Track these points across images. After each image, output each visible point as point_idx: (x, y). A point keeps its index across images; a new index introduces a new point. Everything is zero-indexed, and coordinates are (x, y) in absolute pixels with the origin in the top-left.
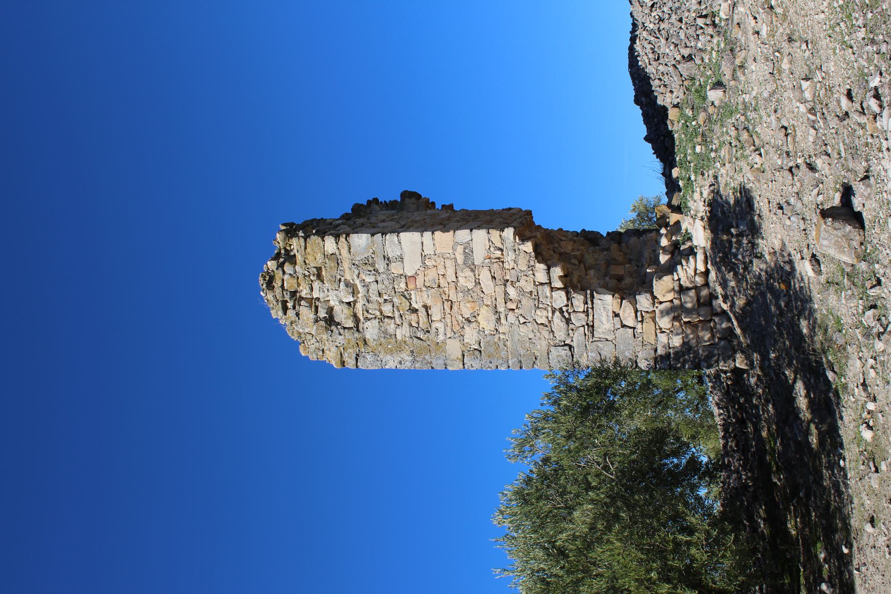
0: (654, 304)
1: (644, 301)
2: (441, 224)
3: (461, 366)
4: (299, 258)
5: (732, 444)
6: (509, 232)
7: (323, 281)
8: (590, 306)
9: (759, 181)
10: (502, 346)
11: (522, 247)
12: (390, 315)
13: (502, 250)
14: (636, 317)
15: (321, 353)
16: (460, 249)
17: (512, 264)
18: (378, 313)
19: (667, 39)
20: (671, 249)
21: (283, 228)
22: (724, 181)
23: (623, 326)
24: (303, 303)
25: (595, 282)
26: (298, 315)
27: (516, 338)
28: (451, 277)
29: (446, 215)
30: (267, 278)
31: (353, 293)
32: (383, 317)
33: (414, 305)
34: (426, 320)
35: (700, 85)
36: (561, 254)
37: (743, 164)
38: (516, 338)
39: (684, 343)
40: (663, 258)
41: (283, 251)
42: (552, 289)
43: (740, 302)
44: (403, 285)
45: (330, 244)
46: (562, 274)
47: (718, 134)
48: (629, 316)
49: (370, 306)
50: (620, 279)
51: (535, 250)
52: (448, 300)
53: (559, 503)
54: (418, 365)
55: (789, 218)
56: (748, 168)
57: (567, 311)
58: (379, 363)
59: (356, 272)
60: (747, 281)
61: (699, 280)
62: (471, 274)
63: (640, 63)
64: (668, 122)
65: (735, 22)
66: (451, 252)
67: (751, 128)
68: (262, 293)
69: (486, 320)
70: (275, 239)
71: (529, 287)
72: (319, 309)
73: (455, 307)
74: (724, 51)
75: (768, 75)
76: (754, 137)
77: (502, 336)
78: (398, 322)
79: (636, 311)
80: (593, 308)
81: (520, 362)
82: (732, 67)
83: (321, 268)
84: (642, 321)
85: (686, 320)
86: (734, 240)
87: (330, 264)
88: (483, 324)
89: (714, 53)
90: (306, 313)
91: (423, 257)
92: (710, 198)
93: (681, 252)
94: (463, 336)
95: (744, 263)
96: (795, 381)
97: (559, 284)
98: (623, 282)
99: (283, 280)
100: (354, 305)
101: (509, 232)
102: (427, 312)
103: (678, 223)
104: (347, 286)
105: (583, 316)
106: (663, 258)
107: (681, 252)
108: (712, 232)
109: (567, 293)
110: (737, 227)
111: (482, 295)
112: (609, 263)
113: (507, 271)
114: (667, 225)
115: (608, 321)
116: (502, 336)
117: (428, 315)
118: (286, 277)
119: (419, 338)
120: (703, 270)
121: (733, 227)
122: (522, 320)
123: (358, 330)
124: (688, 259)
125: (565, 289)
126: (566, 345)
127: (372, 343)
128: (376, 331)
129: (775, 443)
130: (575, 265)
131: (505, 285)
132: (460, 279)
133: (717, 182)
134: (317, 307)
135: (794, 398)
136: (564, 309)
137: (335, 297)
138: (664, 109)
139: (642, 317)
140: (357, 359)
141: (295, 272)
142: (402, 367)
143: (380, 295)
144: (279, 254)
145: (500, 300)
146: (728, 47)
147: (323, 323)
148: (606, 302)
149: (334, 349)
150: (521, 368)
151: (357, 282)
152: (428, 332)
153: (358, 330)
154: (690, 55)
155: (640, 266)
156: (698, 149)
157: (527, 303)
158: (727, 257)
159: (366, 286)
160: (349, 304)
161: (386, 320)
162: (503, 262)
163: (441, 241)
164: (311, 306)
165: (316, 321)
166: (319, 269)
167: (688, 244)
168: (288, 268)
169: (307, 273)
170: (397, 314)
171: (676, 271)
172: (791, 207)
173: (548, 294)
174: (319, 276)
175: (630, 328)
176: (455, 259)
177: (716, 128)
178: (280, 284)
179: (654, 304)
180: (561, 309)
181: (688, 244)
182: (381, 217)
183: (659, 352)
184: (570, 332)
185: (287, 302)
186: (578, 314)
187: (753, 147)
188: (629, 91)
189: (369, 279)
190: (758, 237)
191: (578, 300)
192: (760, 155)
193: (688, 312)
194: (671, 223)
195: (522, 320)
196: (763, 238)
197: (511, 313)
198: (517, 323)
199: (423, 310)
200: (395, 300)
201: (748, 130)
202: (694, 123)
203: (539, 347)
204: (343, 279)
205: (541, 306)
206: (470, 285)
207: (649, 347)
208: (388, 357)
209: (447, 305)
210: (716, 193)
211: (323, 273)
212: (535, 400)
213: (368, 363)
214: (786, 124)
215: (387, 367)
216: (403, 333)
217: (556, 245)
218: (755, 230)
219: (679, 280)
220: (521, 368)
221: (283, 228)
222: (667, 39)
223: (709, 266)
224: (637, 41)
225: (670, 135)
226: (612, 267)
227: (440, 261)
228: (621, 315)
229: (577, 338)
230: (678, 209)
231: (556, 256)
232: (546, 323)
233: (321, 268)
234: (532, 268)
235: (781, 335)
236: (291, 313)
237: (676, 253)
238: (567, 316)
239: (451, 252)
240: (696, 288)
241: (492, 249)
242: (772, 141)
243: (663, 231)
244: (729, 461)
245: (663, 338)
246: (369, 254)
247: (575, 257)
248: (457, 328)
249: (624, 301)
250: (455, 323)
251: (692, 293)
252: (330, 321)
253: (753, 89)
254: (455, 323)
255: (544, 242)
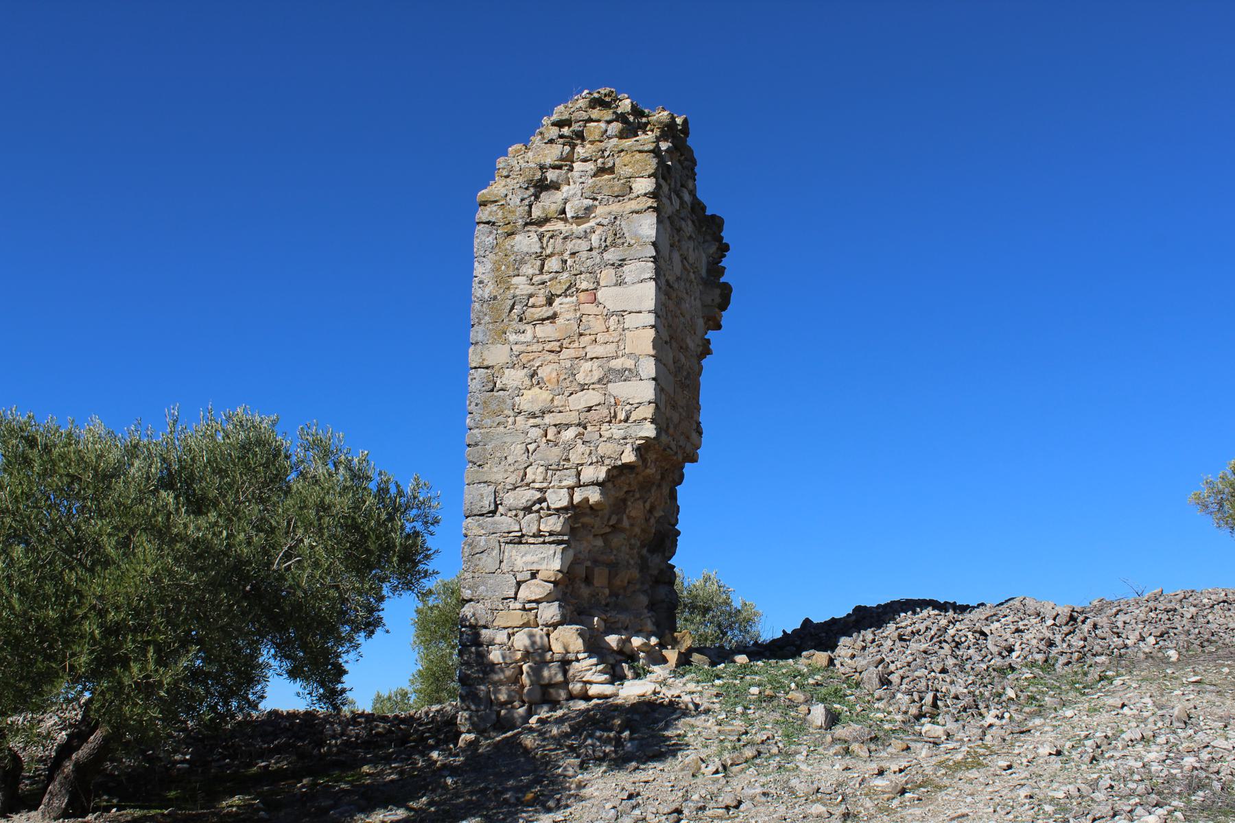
0: (546, 625)
1: (550, 612)
2: (671, 338)
3: (473, 365)
4: (627, 143)
5: (381, 727)
6: (649, 431)
7: (595, 175)
8: (547, 539)
9: (682, 770)
10: (498, 419)
11: (629, 448)
12: (546, 268)
13: (626, 421)
14: (530, 602)
15: (505, 173)
16: (629, 363)
17: (606, 434)
18: (548, 251)
19: (925, 652)
20: (626, 650)
21: (679, 121)
22: (698, 723)
23: (519, 584)
24: (567, 148)
25: (584, 546)
26: (551, 141)
27: (508, 439)
28: (592, 351)
29: (691, 345)
30: (607, 99)
31: (577, 218)
32: (543, 258)
33: (558, 301)
34: (536, 317)
35: (845, 695)
36: (624, 501)
37: (714, 748)
38: (508, 439)
39: (494, 664)
40: (612, 640)
41: (644, 120)
42: (571, 489)
43: (529, 741)
44: (584, 285)
45: (644, 185)
46: (591, 501)
47: (766, 718)
48: (531, 592)
49: (559, 240)
50: (588, 580)
51: (625, 466)
52: (561, 347)
53: (244, 493)
54: (477, 306)
55: (614, 807)
56: (703, 756)
57: (542, 508)
58: (482, 253)
59: (605, 222)
60: (555, 749)
61: (576, 687)
62: (595, 379)
63: (903, 615)
64: (812, 651)
65: (912, 745)
66: (627, 351)
67: (758, 761)
68: (586, 92)
69: (533, 399)
70: (664, 109)
71: (575, 458)
72: (557, 171)
73: (552, 356)
74: (880, 728)
75: (815, 786)
76: (744, 765)
77: (511, 420)
78: (535, 279)
79: (538, 602)
80: (544, 543)
81: (476, 445)
82: (850, 738)
83: (613, 172)
84: (524, 609)
85: (525, 668)
86: (612, 735)
87: (617, 186)
88: (528, 394)
89: (881, 715)
90: (552, 154)
91: (621, 314)
92: (681, 705)
93: (617, 665)
94: (513, 367)
95: (580, 747)
96: (409, 809)
97: (577, 498)
98: (583, 585)
99: (598, 121)
100: (561, 219)
101: (649, 431)
102: (548, 318)
103: (664, 660)
104: (586, 209)
105: (534, 530)
106: (612, 640)
107: (617, 665)
108: (633, 705)
109: (565, 509)
110: (631, 739)
111: (567, 394)
112: (613, 567)
113: (597, 428)
114: (662, 645)
115: (526, 563)
116: (511, 420)
117: (543, 320)
118: (603, 125)
119: (512, 308)
120: (591, 693)
121: (631, 734)
122: (531, 448)
123: (526, 224)
124: (605, 673)
125: (571, 507)
126: (496, 506)
127: (508, 243)
128: (525, 249)
129: (346, 783)
130: (609, 519)
131: (579, 425)
132: (590, 363)
133: (700, 713)
134: (560, 167)
135: (386, 808)
136: (544, 505)
137: (571, 194)
138: (833, 647)
139: (530, 610)
140: (488, 223)
141: (609, 138)
142: (475, 285)
143: (573, 254)
144: (642, 114)
145: (559, 418)
146: (881, 734)
147: (538, 176)
148: (551, 562)
149: (503, 191)
150: (469, 445)
151: (592, 223)
152: (521, 320)
153: (526, 224)
154: (890, 683)
155: (606, 608)
156: (755, 690)
157: (554, 454)
158: (593, 724)
159: (586, 235)
160: (563, 212)
161: (539, 263)
162: (610, 422)
163: (642, 339)
164: (562, 159)
165: (542, 168)
166: (611, 170)
167: (629, 674)
168: (616, 127)
169: (606, 154)
170: (546, 277)
171: (590, 657)
172: (629, 810)
173: (564, 483)
174: (601, 171)
175: (516, 594)
176: (617, 357)
177: (777, 716)
178: (593, 117)
179: (546, 625)
180: (545, 500)
181: (629, 674)
182: (692, 257)
183: (483, 632)
184: (514, 513)
185: (570, 126)
186: (536, 523)
187: (729, 762)
188: (874, 599)
189: (595, 238)
190: (609, 766)
191: (554, 524)
192: (717, 772)
193: (536, 672)
194: (664, 652)
195: (531, 448)
196: (605, 772)
197: (541, 432)
198: (528, 441)
199: (550, 313)
200: (565, 275)
201: (755, 757)
202: (793, 685)
203: (495, 470)
204: (597, 203)
205: (550, 472)
206: (580, 378)
207: (490, 618)
208: (489, 266)
209: (555, 346)
210: (685, 713)
211: (606, 177)
212: (394, 464)
213: (483, 238)
214: (742, 807)
215: (476, 264)
216: (521, 285)
217: (637, 495)
218: (619, 762)
219: (578, 660)
220: (469, 445)
221: (679, 121)
222: (925, 652)
223: (595, 701)
224: (937, 612)
225: (796, 654)
226: (606, 571)
227: (614, 336)
228: (533, 581)
229: (504, 522)
230: (684, 660)
231: (621, 494)
232: (527, 480)
233: (613, 172)
234: (601, 461)
235: (472, 793)
236: (554, 132)
237: (619, 658)
238: (534, 508)
239: (627, 351)
240: (566, 682)
241: (628, 407)
242: (729, 789)
243: (654, 640)
244: (360, 723)
245: (501, 637)
246: (628, 239)
247: (620, 521)
248: (524, 358)
249: (551, 585)
250: (531, 356)
251: (560, 678)
252: (541, 186)
253: (809, 765)
254: (531, 356)
255: (640, 478)
